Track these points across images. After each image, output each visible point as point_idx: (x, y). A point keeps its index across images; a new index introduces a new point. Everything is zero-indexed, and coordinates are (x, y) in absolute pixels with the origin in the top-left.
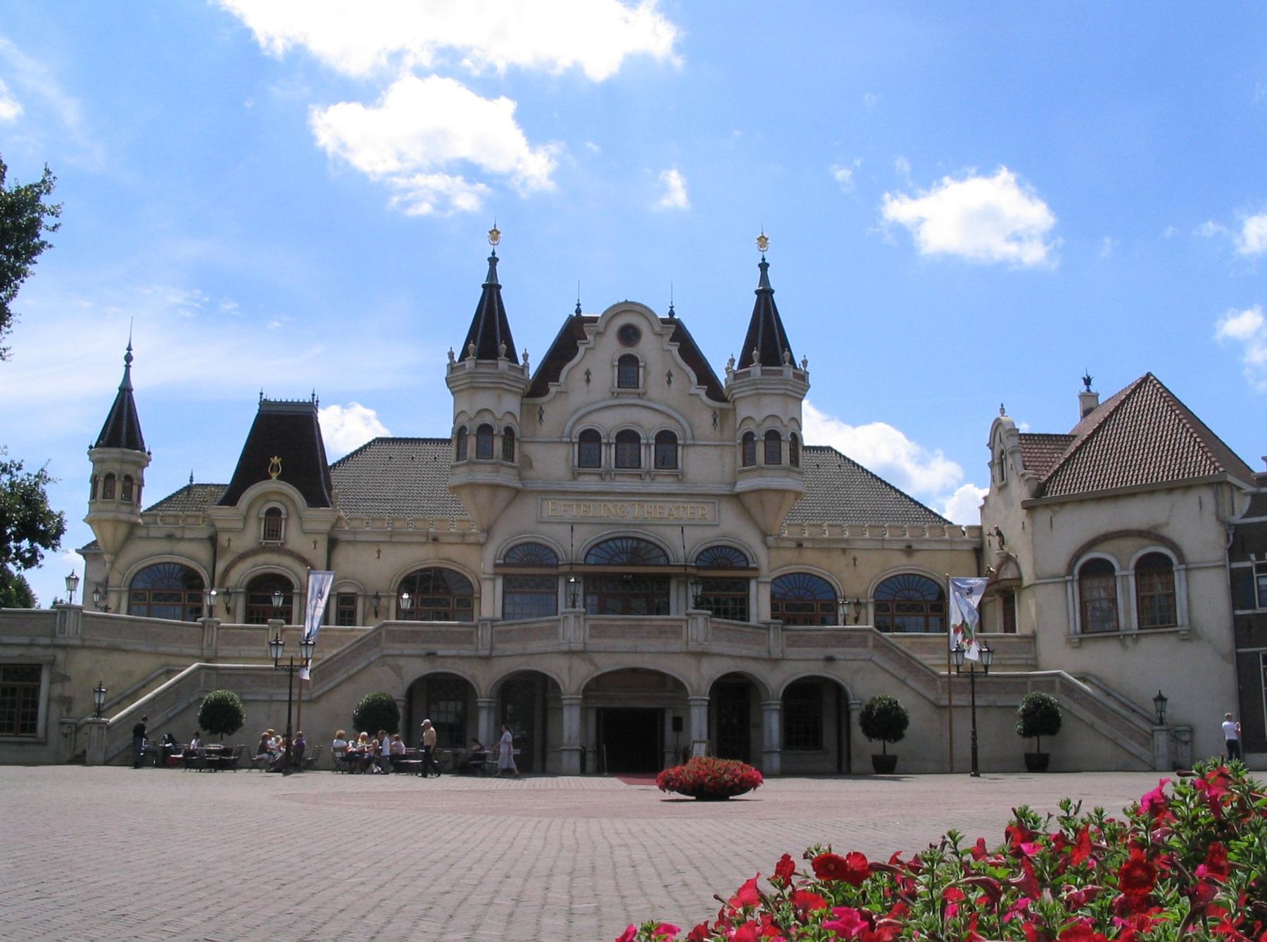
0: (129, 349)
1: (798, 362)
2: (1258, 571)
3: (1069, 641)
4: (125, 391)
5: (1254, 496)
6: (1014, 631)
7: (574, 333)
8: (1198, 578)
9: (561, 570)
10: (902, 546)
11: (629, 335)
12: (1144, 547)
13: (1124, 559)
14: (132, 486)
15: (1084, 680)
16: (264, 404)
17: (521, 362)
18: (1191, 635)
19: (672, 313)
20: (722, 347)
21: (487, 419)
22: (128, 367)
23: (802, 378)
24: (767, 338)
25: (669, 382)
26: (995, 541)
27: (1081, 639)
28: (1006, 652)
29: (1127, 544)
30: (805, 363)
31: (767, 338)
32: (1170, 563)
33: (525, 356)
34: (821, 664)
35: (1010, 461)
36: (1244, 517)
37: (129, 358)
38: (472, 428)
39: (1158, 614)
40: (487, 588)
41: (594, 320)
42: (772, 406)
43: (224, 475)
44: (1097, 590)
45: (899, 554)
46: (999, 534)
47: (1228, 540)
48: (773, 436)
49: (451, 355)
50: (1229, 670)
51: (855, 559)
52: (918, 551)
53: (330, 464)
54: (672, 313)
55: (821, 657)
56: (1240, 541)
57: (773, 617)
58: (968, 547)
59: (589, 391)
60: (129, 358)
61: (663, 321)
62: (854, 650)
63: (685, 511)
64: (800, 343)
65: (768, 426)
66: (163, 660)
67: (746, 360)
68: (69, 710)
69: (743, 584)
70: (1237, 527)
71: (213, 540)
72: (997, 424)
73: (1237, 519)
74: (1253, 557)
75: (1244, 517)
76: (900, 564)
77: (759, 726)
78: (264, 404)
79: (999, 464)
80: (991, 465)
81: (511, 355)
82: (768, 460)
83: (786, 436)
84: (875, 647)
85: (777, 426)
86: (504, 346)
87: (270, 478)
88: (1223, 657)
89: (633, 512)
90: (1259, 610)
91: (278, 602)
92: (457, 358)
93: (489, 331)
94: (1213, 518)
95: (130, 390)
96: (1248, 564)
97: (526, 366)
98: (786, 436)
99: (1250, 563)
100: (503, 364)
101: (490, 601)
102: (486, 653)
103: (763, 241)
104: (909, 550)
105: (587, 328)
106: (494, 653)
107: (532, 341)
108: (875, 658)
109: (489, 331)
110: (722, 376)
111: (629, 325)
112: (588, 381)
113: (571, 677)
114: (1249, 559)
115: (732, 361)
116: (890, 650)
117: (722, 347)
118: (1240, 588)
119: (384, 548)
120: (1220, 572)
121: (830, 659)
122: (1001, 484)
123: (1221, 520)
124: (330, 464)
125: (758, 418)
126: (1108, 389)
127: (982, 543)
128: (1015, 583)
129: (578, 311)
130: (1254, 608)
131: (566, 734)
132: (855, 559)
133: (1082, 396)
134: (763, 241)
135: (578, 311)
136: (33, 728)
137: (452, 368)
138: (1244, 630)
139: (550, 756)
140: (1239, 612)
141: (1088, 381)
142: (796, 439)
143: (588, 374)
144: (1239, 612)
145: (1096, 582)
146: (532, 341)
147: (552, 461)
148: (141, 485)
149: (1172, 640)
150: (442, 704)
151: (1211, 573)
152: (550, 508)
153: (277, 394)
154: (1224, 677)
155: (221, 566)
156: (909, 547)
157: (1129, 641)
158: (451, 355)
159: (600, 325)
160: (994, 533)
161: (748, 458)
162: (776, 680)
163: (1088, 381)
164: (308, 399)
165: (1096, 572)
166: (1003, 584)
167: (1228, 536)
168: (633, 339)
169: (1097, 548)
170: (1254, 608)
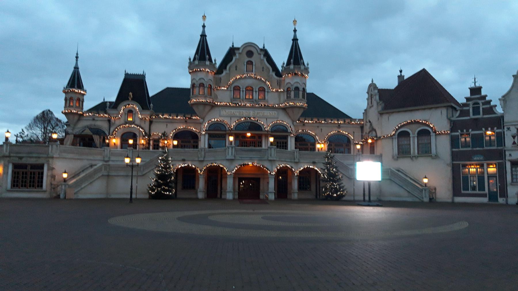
0: (77, 54)
1: (306, 64)
3: (393, 157)
4: (76, 68)
5: (461, 111)
7: (232, 52)
8: (440, 138)
9: (227, 132)
11: (250, 54)
12: (420, 127)
13: (413, 131)
14: (80, 101)
15: (398, 171)
16: (127, 75)
17: (214, 62)
18: (436, 157)
19: (264, 47)
20: (280, 58)
21: (202, 81)
22: (77, 60)
23: (307, 70)
24: (295, 56)
25: (263, 70)
26: (368, 124)
27: (398, 157)
29: (414, 126)
30: (308, 64)
31: (295, 56)
32: (430, 133)
33: (215, 61)
35: (374, 97)
37: (77, 57)
38: (197, 84)
39: (425, 151)
40: (202, 138)
41: (238, 49)
42: (297, 79)
43: (113, 99)
44: (404, 141)
46: (370, 122)
47: (451, 125)
48: (297, 89)
49: (190, 59)
50: (449, 169)
53: (151, 94)
54: (264, 47)
56: (454, 126)
57: (296, 148)
59: (236, 76)
60: (77, 57)
61: (261, 50)
63: (267, 113)
64: (306, 59)
65: (295, 85)
66: (90, 162)
67: (289, 63)
68: (54, 180)
69: (286, 138)
70: (454, 121)
71: (109, 121)
72: (370, 86)
73: (454, 119)
74: (459, 131)
77: (291, 184)
78: (127, 75)
79: (371, 97)
80: (368, 99)
81: (210, 59)
82: (295, 96)
83: (301, 89)
85: (298, 85)
86: (207, 56)
87: (128, 99)
88: (447, 165)
89: (251, 113)
91: (131, 142)
92: (192, 60)
93: (203, 51)
94: (446, 118)
95: (78, 68)
96: (458, 134)
97: (216, 63)
98: (301, 89)
100: (208, 63)
101: (204, 142)
102: (202, 159)
103: (295, 22)
105: (236, 52)
106: (206, 159)
107: (218, 56)
109: (203, 51)
110: (280, 69)
111: (250, 50)
112: (236, 69)
113: (230, 169)
114: (458, 132)
115: (284, 64)
117: (280, 58)
118: (454, 142)
119: (169, 125)
122: (370, 105)
123: (449, 119)
124: (151, 94)
125: (292, 83)
126: (407, 74)
129: (233, 46)
131: (228, 188)
133: (399, 77)
134: (295, 22)
135: (233, 46)
136: (42, 186)
137: (190, 63)
138: (455, 156)
139: (223, 193)
140: (454, 150)
141: (401, 71)
142: (304, 90)
143: (236, 67)
145: (403, 139)
146: (218, 56)
147: (223, 95)
148: (83, 101)
149: (429, 159)
151: (438, 140)
152: (224, 112)
153: (131, 71)
154: (448, 172)
155: (112, 129)
157: (414, 158)
158: (190, 59)
159: (240, 51)
161: (288, 98)
162: (297, 170)
163: (401, 71)
164: (142, 73)
165: (403, 135)
168: (250, 55)
169: (406, 126)
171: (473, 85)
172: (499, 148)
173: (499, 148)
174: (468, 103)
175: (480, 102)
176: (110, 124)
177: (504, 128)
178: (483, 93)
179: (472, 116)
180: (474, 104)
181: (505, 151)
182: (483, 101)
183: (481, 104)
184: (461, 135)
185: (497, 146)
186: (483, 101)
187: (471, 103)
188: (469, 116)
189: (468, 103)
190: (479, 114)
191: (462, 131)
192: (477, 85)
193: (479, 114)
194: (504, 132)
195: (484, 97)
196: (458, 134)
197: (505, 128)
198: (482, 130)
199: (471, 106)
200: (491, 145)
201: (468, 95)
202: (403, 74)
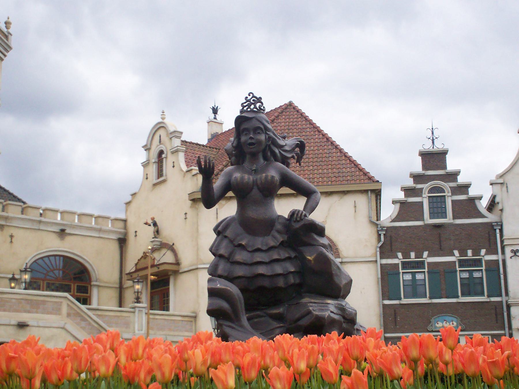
2: (403, 268)
6: (168, 309)
10: (57, 229)
28: (170, 330)
34: (11, 330)
36: (393, 221)
45: (54, 237)
46: (155, 224)
47: (379, 240)
51: (12, 236)
52: (70, 234)
55: (14, 322)
56: (390, 241)
58: (115, 237)
62: (48, 316)
70: (389, 230)
74: (400, 255)
75: (393, 221)
76: (53, 245)
84: (69, 315)
90: (405, 301)
96: (395, 261)
99: (398, 260)
104: (62, 233)
108: (69, 327)
114: (453, 255)
116: (84, 319)
120: (371, 266)
121: (22, 326)
127: (126, 234)
128: (174, 268)
130: (400, 299)
132: (12, 236)
140: (387, 302)
144: (387, 302)
150: (213, 177)
156: (63, 231)
160: (150, 222)
166: (162, 268)
167: (379, 235)
170: (457, 297)
171: (428, 146)
172: (493, 299)
173: (493, 299)
174: (419, 186)
175: (447, 186)
176: (63, 370)
177: (503, 252)
178: (451, 165)
179: (428, 220)
180: (431, 191)
181: (509, 307)
182: (453, 184)
183: (448, 193)
184: (405, 265)
185: (489, 296)
186: (453, 184)
187: (426, 187)
188: (421, 218)
189: (419, 186)
190: (444, 215)
191: (406, 255)
192: (439, 146)
193: (444, 215)
194: (504, 261)
195: (453, 176)
196: (395, 261)
197: (508, 250)
198: (453, 255)
199: (426, 194)
200: (415, 295)
201: (417, 167)
202: (165, 121)
